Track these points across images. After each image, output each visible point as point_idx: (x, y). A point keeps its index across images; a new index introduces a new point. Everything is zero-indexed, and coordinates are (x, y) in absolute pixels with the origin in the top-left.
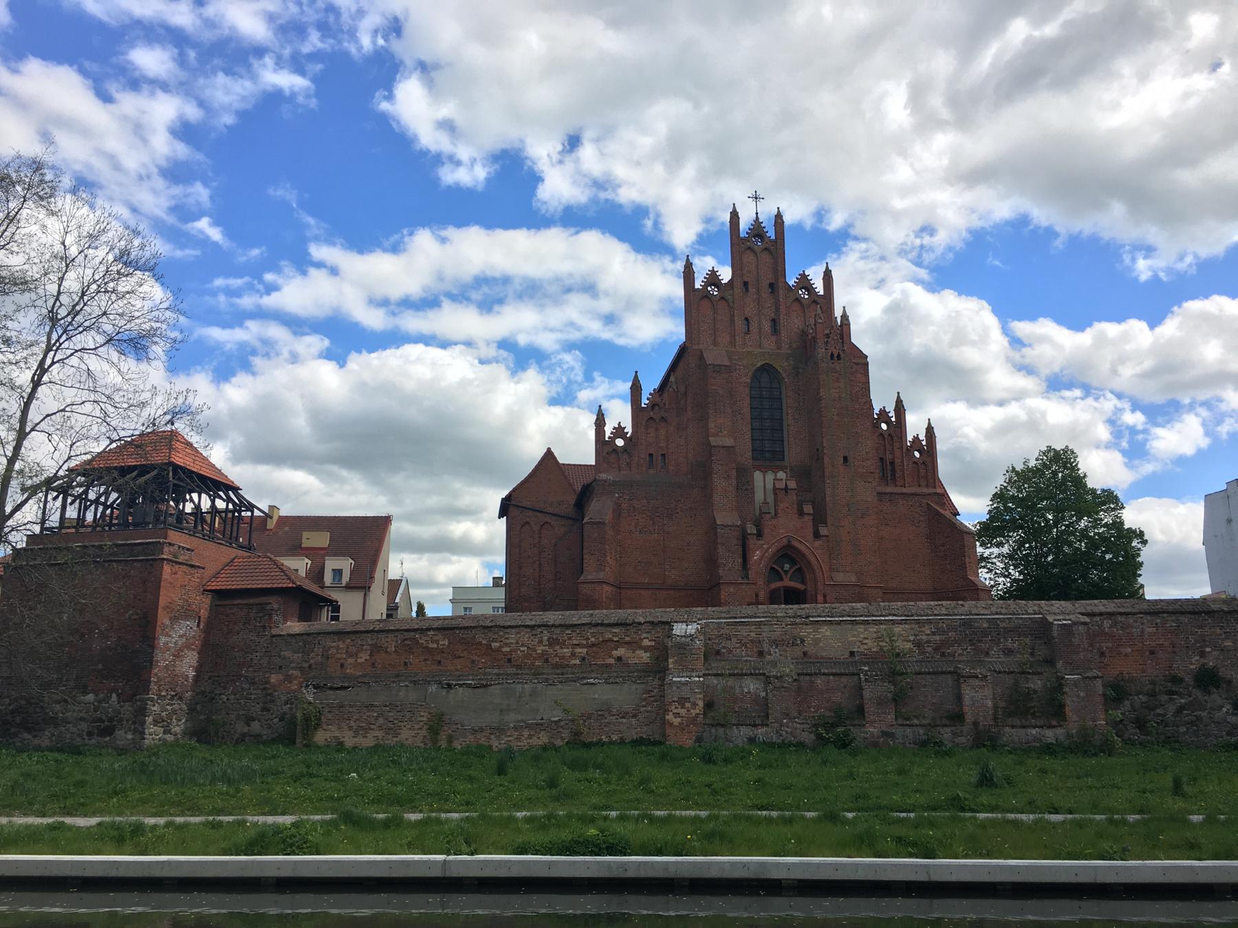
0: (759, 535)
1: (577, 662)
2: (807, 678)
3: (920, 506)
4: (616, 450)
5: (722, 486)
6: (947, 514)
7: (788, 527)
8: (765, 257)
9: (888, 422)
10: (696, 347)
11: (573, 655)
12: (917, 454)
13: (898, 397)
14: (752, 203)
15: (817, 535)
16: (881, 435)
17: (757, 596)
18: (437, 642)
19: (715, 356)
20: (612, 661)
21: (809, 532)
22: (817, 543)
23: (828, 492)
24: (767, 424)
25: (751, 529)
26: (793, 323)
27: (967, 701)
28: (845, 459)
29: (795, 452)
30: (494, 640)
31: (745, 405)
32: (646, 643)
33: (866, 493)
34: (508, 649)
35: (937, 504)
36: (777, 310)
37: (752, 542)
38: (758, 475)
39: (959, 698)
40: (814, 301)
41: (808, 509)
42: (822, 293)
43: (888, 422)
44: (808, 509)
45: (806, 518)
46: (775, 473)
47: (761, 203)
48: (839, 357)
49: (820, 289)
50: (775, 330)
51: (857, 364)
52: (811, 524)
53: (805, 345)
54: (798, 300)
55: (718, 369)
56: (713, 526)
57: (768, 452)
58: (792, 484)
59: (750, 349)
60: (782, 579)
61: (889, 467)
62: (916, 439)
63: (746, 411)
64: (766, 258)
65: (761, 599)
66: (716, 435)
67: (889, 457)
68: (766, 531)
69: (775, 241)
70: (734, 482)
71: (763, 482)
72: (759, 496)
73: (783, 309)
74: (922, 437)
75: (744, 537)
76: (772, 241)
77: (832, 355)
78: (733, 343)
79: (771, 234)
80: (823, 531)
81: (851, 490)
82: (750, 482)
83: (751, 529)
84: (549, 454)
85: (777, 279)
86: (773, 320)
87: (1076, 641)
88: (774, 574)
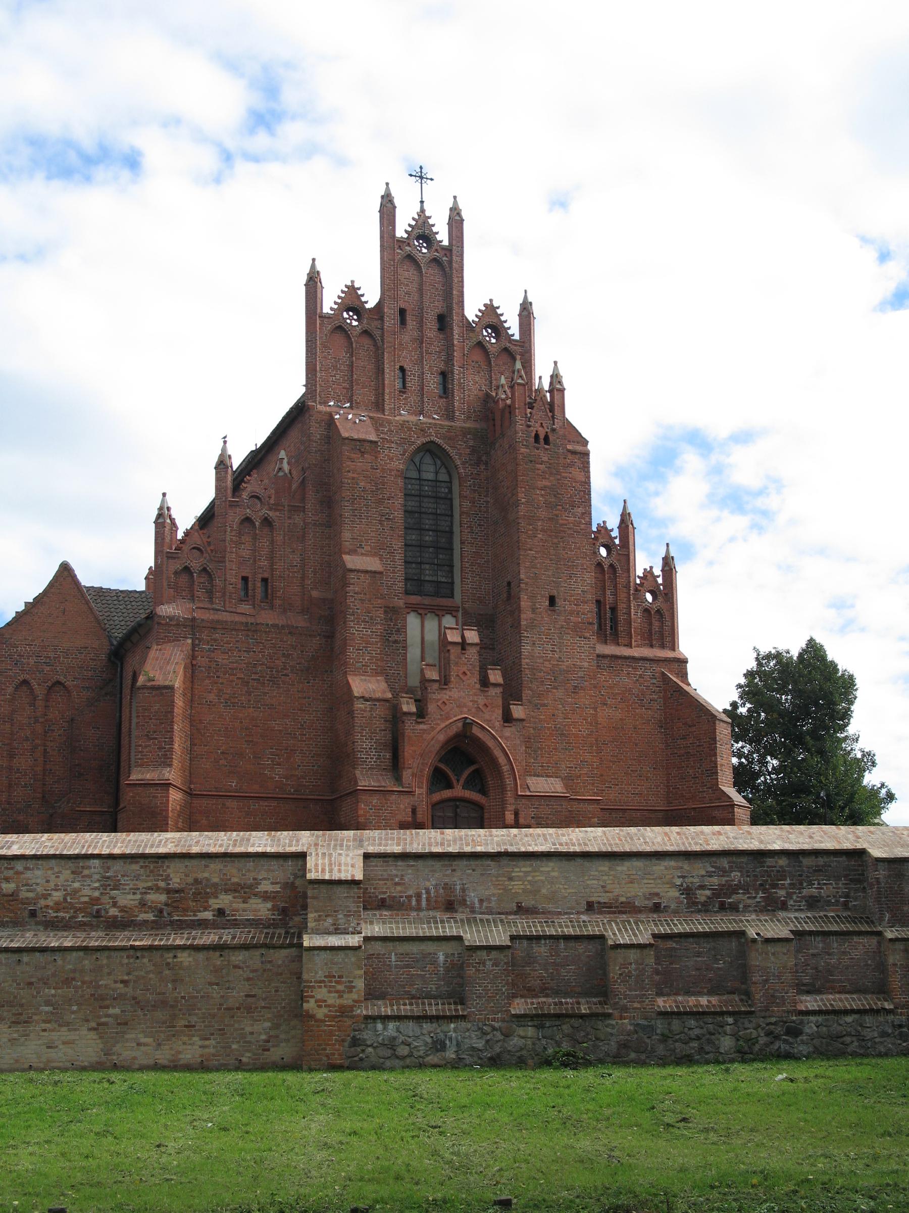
0: (421, 714)
1: (150, 917)
7: (464, 702)
11: (143, 904)
14: (414, 184)
15: (508, 718)
16: (599, 565)
17: (414, 811)
19: (352, 422)
20: (208, 915)
22: (508, 732)
24: (428, 538)
25: (408, 706)
26: (470, 384)
28: (552, 600)
35: (677, 675)
36: (449, 360)
37: (411, 728)
38: (413, 621)
40: (506, 349)
41: (495, 676)
42: (517, 337)
44: (495, 676)
45: (494, 692)
46: (439, 617)
47: (428, 186)
48: (547, 440)
49: (514, 330)
50: (446, 391)
51: (574, 453)
53: (493, 418)
55: (360, 445)
56: (342, 699)
57: (428, 587)
58: (472, 636)
60: (449, 786)
63: (398, 515)
64: (432, 275)
65: (420, 817)
67: (609, 598)
68: (431, 708)
69: (448, 250)
71: (418, 630)
74: (657, 571)
75: (396, 718)
76: (444, 248)
77: (537, 437)
78: (379, 405)
79: (443, 236)
80: (518, 711)
81: (556, 645)
82: (402, 630)
83: (408, 706)
84: (65, 572)
85: (450, 309)
86: (443, 374)
88: (439, 779)
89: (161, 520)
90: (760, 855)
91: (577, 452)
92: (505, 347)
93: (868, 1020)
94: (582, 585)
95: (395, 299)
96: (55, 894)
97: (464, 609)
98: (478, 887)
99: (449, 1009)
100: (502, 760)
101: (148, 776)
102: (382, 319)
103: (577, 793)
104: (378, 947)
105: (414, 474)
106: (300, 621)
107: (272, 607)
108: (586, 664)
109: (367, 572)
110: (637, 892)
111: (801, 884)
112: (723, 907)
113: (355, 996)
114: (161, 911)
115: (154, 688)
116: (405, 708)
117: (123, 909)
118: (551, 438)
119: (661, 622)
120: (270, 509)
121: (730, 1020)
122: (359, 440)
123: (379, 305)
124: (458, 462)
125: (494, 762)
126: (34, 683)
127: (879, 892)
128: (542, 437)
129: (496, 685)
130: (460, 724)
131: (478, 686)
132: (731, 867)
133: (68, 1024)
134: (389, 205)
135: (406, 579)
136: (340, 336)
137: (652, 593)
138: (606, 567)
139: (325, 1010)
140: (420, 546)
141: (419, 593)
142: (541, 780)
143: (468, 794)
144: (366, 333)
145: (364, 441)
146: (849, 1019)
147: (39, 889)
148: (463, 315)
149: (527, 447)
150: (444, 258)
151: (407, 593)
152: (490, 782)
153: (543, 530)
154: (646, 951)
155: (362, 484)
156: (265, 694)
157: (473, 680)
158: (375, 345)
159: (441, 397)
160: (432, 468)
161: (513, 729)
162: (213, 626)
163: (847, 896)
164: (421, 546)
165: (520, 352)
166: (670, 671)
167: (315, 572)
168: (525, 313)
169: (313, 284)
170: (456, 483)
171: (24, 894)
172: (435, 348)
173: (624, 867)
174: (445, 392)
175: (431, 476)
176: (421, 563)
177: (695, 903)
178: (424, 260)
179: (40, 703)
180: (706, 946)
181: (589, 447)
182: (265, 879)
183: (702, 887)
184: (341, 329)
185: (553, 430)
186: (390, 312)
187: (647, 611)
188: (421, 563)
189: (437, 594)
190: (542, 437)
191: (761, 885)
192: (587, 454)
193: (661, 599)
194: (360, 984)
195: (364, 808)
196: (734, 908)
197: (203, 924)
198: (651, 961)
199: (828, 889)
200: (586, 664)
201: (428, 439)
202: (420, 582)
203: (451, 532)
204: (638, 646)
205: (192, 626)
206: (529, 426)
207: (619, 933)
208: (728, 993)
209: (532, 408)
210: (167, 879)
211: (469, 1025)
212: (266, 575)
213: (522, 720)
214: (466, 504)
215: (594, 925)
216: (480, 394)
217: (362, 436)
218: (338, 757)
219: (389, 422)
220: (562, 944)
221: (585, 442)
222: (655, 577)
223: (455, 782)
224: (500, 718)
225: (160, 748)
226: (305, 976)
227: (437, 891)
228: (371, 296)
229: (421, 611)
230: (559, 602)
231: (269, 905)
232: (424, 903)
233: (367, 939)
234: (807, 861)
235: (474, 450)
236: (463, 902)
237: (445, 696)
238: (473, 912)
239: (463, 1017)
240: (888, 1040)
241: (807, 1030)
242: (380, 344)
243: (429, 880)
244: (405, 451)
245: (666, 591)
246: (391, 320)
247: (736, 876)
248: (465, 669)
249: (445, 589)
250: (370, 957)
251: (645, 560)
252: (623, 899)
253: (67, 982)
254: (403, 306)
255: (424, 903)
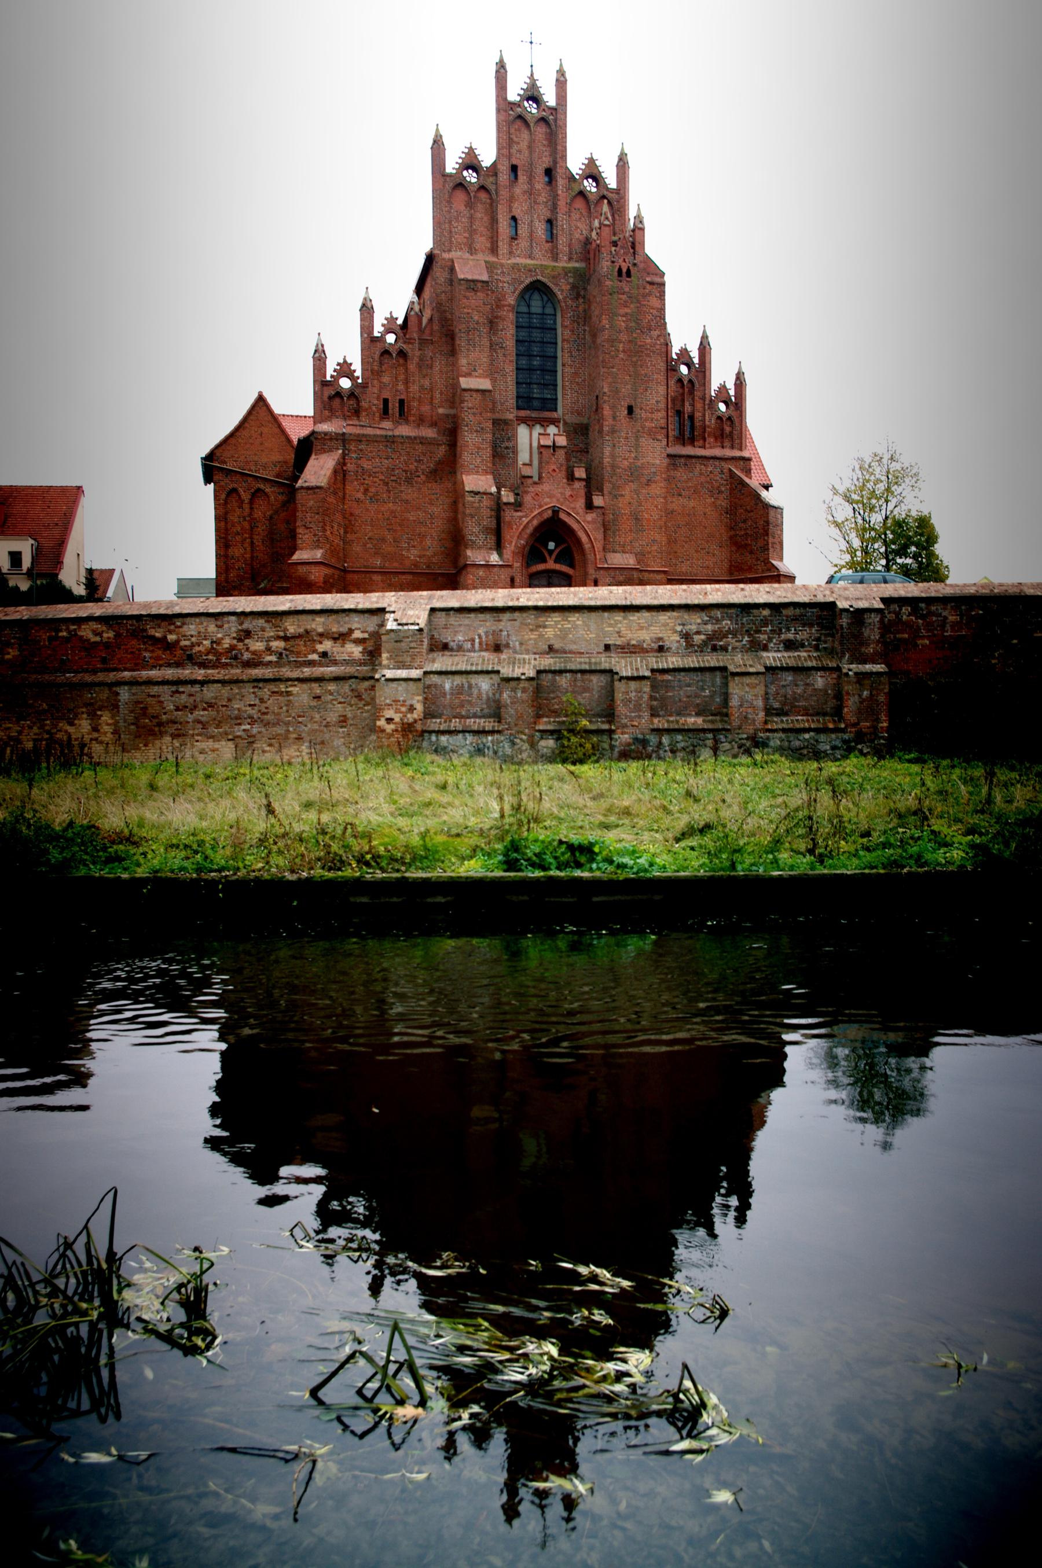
0: (518, 505)
1: (273, 658)
2: (550, 676)
3: (722, 472)
4: (339, 394)
5: (474, 442)
6: (754, 482)
7: (555, 494)
8: (541, 131)
9: (689, 365)
10: (446, 256)
11: (268, 648)
12: (722, 407)
13: (704, 331)
15: (590, 506)
16: (680, 381)
18: (100, 634)
20: (315, 657)
21: (581, 503)
22: (590, 517)
23: (607, 451)
26: (574, 227)
27: (734, 702)
28: (630, 410)
29: (565, 400)
30: (170, 632)
31: (508, 334)
32: (357, 634)
33: (654, 454)
34: (187, 643)
36: (554, 208)
37: (508, 514)
38: (523, 431)
39: (726, 697)
43: (689, 365)
44: (580, 473)
45: (577, 485)
48: (629, 274)
49: (612, 182)
50: (552, 237)
51: (651, 283)
52: (582, 492)
54: (582, 194)
55: (472, 285)
56: (456, 496)
57: (536, 400)
58: (562, 441)
59: (518, 260)
60: (545, 561)
61: (687, 423)
62: (723, 388)
63: (510, 344)
66: (468, 375)
68: (528, 499)
69: (553, 110)
70: (489, 436)
71: (526, 439)
72: (523, 457)
73: (562, 203)
75: (498, 508)
76: (550, 108)
77: (620, 270)
78: (494, 250)
79: (550, 98)
80: (598, 501)
81: (638, 451)
85: (555, 162)
86: (550, 222)
87: (866, 632)
89: (317, 355)
90: (746, 608)
91: (653, 282)
92: (604, 199)
93: (822, 737)
94: (656, 395)
95: (510, 156)
96: (205, 642)
97: (564, 420)
98: (458, 633)
99: (489, 724)
100: (584, 539)
101: (305, 557)
102: (496, 175)
103: (648, 566)
104: (435, 679)
105: (525, 309)
106: (429, 433)
107: (407, 421)
108: (658, 462)
109: (477, 391)
110: (646, 636)
111: (780, 630)
112: (714, 649)
113: (415, 716)
114: (281, 654)
115: (308, 488)
116: (505, 500)
117: (254, 653)
118: (633, 270)
119: (731, 426)
120: (405, 343)
121: (710, 736)
122: (473, 281)
123: (494, 164)
124: (560, 297)
125: (578, 541)
126: (241, 490)
127: (842, 636)
128: (624, 270)
129: (580, 479)
130: (550, 512)
131: (565, 481)
132: (723, 617)
133: (212, 737)
134: (502, 70)
135: (518, 397)
136: (463, 194)
137: (726, 403)
138: (685, 383)
139: (392, 726)
140: (529, 369)
141: (530, 408)
142: (618, 555)
143: (557, 567)
144: (483, 188)
145: (477, 281)
146: (807, 736)
147: (194, 639)
148: (567, 168)
149: (611, 280)
150: (551, 117)
151: (518, 408)
152: (577, 557)
153: (623, 351)
154: (644, 682)
155: (476, 318)
156: (401, 492)
157: (562, 475)
158: (491, 199)
159: (547, 242)
160: (539, 303)
161: (594, 515)
162: (359, 439)
163: (818, 639)
164: (531, 370)
165: (615, 200)
166: (736, 467)
167: (441, 393)
168: (621, 163)
169: (438, 147)
170: (559, 315)
171: (183, 643)
172: (542, 199)
173: (634, 617)
174: (552, 238)
175: (539, 311)
176: (530, 384)
177: (692, 646)
178: (533, 122)
179: (246, 506)
180: (696, 677)
181: (666, 278)
182: (357, 629)
183: (698, 633)
184: (461, 185)
185: (635, 265)
186: (504, 169)
187: (719, 418)
188: (530, 384)
189: (542, 409)
190: (624, 270)
191: (747, 631)
192: (663, 284)
193: (732, 408)
194: (419, 707)
195: (470, 577)
196: (724, 649)
197: (312, 663)
198: (647, 689)
199: (803, 635)
200: (658, 462)
201: (535, 278)
202: (529, 399)
203: (556, 357)
204: (711, 448)
205: (342, 439)
206: (613, 262)
207: (624, 667)
208: (712, 715)
209: (616, 246)
210: (285, 630)
211: (502, 738)
212: (402, 397)
213: (602, 508)
214: (567, 332)
215: (605, 662)
216: (581, 238)
217: (476, 277)
218: (456, 540)
219: (502, 265)
220: (579, 675)
221: (663, 274)
222: (727, 390)
223: (548, 557)
224: (583, 506)
225: (315, 535)
226: (378, 701)
227: (487, 637)
228: (487, 157)
229: (530, 422)
230: (637, 410)
231: (360, 649)
232: (477, 645)
233: (426, 673)
234: (789, 612)
235: (574, 287)
236: (507, 646)
237: (539, 489)
238: (515, 652)
239: (499, 732)
240: (837, 752)
241: (772, 743)
242: (494, 197)
243: (483, 627)
244: (516, 289)
245: (738, 405)
246: (504, 176)
247: (726, 623)
248: (554, 467)
249: (550, 404)
250: (429, 687)
251: (721, 376)
252: (634, 642)
253: (211, 705)
254: (514, 163)
255: (477, 645)
